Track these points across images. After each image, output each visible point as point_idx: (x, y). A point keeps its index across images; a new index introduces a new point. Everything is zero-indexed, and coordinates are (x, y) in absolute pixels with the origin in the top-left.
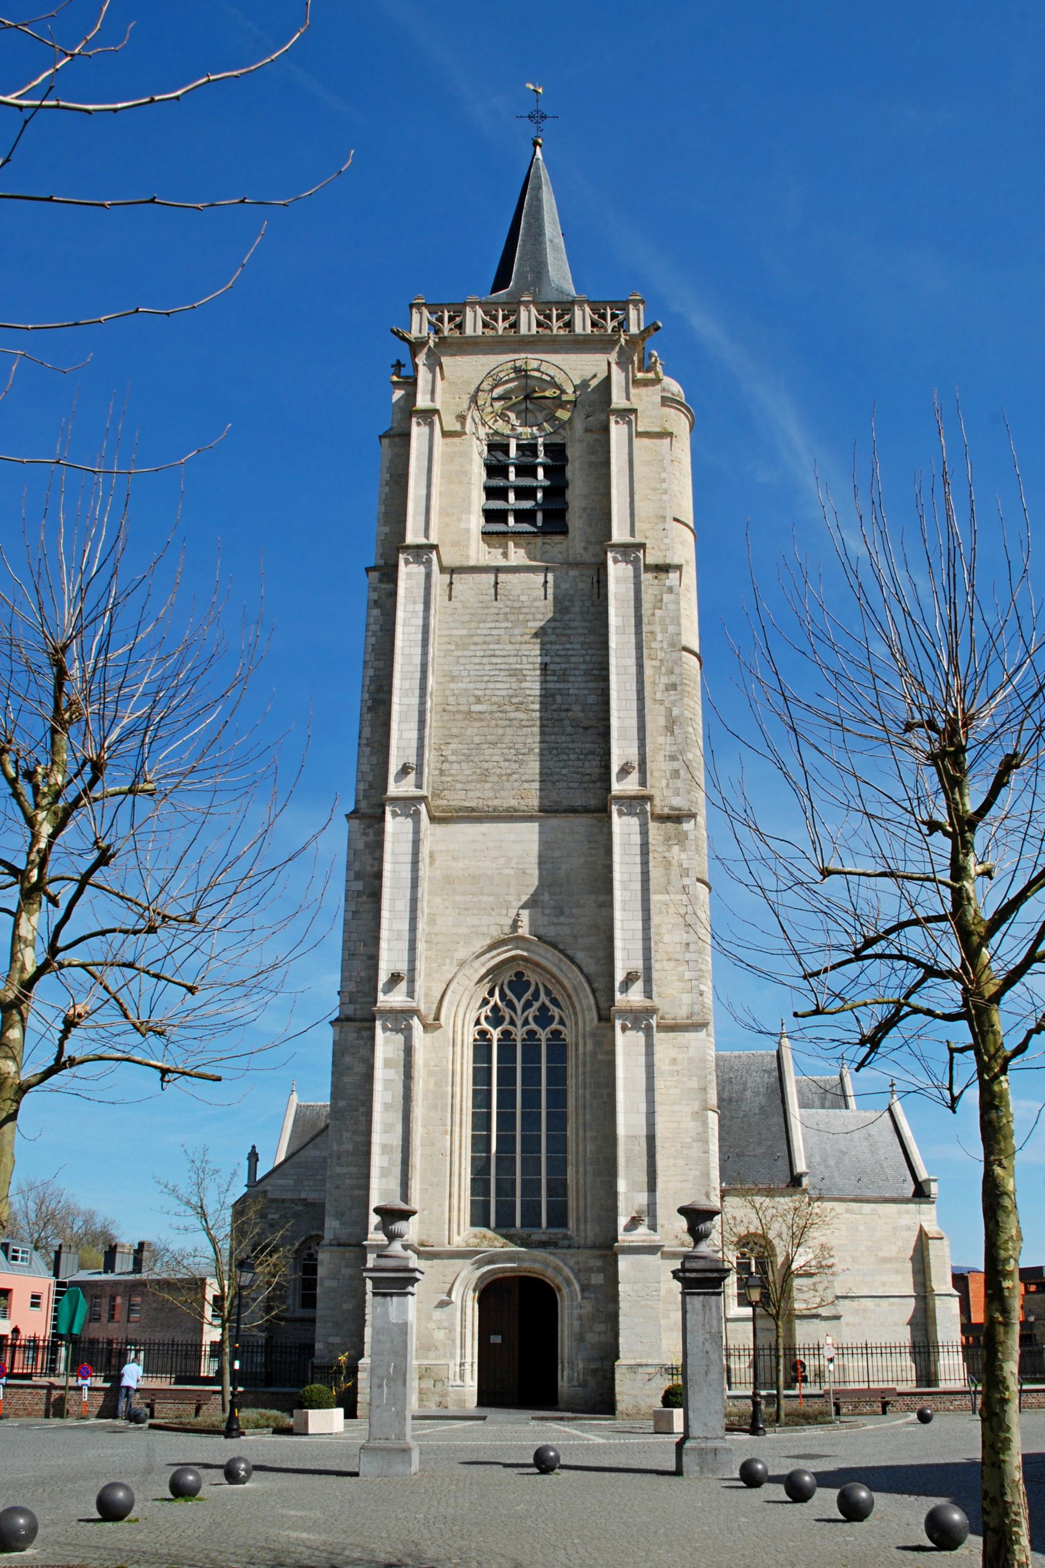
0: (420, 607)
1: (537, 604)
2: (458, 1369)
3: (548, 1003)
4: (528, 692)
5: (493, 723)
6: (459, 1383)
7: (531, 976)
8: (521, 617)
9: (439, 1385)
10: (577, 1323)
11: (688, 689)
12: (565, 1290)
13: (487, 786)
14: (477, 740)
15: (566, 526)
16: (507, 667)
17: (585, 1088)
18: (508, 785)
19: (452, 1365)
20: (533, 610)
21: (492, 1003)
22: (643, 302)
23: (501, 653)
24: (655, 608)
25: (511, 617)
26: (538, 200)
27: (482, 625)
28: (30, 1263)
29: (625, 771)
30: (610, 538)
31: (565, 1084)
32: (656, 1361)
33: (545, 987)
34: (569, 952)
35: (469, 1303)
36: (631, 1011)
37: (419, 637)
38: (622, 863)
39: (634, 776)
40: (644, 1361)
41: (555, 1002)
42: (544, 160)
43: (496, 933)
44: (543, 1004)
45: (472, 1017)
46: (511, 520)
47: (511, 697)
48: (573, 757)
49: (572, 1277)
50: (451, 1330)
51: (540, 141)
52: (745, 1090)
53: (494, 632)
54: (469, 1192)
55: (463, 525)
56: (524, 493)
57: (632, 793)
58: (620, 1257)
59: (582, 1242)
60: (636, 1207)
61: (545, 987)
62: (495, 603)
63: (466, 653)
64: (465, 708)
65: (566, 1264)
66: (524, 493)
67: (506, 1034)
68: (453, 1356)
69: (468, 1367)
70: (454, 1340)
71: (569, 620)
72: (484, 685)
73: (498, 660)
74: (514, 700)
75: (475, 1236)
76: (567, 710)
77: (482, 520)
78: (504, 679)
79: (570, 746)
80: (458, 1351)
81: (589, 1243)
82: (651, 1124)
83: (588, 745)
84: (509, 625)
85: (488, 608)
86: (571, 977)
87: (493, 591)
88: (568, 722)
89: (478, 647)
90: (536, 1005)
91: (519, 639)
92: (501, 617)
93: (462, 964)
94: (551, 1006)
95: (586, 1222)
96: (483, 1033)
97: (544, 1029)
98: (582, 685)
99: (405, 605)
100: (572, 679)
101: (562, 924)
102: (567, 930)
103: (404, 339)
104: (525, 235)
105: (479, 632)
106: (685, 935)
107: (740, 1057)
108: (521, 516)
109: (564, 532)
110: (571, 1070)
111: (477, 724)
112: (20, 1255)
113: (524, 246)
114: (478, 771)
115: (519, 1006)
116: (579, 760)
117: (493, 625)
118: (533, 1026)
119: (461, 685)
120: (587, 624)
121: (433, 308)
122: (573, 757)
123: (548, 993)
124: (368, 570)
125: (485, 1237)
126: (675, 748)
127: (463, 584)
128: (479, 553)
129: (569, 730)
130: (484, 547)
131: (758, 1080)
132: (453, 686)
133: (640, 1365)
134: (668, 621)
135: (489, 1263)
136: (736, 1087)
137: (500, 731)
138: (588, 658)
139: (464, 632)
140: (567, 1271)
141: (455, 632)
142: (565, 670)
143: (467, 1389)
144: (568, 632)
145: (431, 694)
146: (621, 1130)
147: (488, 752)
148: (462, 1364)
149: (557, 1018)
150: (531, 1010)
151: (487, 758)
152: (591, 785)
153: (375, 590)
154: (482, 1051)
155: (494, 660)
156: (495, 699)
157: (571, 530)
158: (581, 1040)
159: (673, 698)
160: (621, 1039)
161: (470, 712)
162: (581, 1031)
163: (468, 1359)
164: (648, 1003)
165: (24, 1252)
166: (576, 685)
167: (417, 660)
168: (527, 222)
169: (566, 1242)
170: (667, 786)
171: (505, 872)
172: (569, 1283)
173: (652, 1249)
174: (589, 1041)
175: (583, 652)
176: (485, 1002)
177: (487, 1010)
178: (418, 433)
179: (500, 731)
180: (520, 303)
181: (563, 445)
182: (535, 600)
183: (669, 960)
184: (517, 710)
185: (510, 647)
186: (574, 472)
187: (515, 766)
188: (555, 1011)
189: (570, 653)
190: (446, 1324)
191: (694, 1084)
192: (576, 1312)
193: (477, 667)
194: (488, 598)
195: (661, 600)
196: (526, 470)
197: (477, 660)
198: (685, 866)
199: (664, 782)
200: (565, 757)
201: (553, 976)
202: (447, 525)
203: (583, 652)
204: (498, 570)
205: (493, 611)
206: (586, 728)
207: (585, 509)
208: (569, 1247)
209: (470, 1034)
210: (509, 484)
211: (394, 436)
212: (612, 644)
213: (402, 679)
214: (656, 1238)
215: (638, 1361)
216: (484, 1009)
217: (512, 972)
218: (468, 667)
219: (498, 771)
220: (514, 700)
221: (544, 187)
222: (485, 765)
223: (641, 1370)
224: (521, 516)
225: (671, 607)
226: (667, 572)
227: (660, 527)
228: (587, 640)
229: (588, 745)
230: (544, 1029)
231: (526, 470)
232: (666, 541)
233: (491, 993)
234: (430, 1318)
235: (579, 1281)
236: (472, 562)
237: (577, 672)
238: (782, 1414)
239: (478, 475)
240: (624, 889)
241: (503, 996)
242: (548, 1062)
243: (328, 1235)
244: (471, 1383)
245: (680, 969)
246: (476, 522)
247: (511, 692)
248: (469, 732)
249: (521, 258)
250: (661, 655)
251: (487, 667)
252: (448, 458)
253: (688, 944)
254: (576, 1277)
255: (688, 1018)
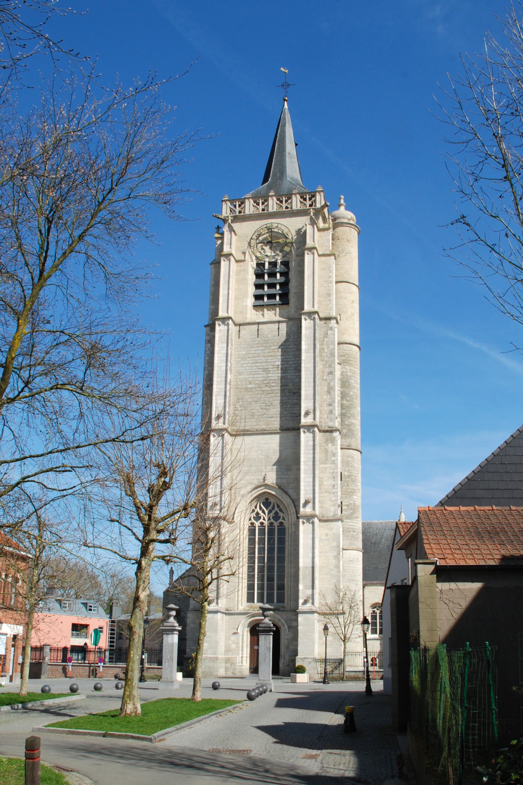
0: (225, 345)
1: (275, 338)
2: (240, 659)
3: (278, 511)
4: (271, 378)
5: (256, 392)
6: (240, 664)
7: (272, 500)
8: (268, 345)
9: (233, 665)
10: (286, 641)
11: (351, 362)
12: (282, 628)
13: (254, 420)
14: (250, 400)
15: (288, 300)
16: (262, 367)
17: (291, 546)
18: (262, 419)
19: (238, 657)
20: (273, 341)
21: (256, 511)
22: (322, 191)
23: (260, 361)
24: (324, 337)
25: (264, 345)
26: (284, 132)
27: (252, 349)
28: (98, 612)
29: (307, 414)
30: (303, 309)
31: (285, 544)
32: (312, 657)
33: (277, 505)
34: (286, 490)
35: (245, 633)
36: (306, 516)
37: (225, 358)
38: (304, 454)
39: (311, 416)
40: (307, 657)
41: (281, 510)
42: (289, 109)
43: (256, 483)
44: (276, 512)
45: (248, 517)
46: (266, 299)
47: (264, 380)
48: (289, 406)
49: (284, 622)
50: (238, 644)
51: (286, 98)
52: (382, 538)
53: (257, 352)
54: (246, 589)
55: (244, 304)
56: (272, 286)
57: (309, 424)
58: (299, 615)
59: (289, 609)
60: (306, 596)
61: (277, 505)
62: (258, 339)
63: (246, 362)
64: (244, 386)
65: (282, 618)
66: (272, 286)
67: (262, 523)
68: (238, 654)
69: (244, 658)
70: (239, 648)
71: (289, 345)
72: (252, 376)
73: (259, 365)
74: (265, 382)
75: (248, 607)
76: (287, 386)
77: (253, 300)
78: (261, 373)
79: (288, 401)
80: (241, 652)
81: (292, 609)
82: (313, 562)
83: (295, 401)
84: (263, 348)
85: (255, 341)
86: (286, 501)
87: (257, 333)
88: (287, 391)
89: (250, 359)
90: (274, 512)
91: (267, 354)
92: (260, 345)
93: (243, 496)
94: (279, 512)
95: (291, 601)
96: (252, 524)
97: (276, 521)
98: (293, 374)
99: (219, 344)
100: (289, 371)
101: (283, 478)
102: (285, 481)
103: (219, 218)
104: (277, 152)
105: (251, 352)
106: (333, 482)
107: (382, 523)
108: (271, 297)
109: (288, 304)
110: (287, 539)
111: (250, 393)
112: (93, 608)
113: (276, 157)
114: (250, 414)
115: (266, 512)
116: (291, 407)
117: (256, 349)
118: (272, 520)
119: (243, 376)
120: (295, 346)
121: (232, 201)
122: (289, 406)
123: (278, 506)
124: (206, 326)
125: (252, 607)
126: (331, 400)
127: (245, 330)
128: (253, 315)
129: (287, 394)
130: (254, 312)
131: (389, 533)
132: (240, 377)
133: (306, 658)
134: (330, 343)
135: (253, 617)
136: (378, 537)
137: (259, 396)
138: (296, 362)
139: (244, 353)
140: (283, 621)
141: (241, 353)
142: (286, 368)
143: (244, 667)
144: (288, 350)
145: (230, 382)
146: (301, 564)
147: (254, 405)
148: (242, 657)
149: (282, 517)
150: (271, 514)
151: (254, 408)
152: (296, 418)
153: (208, 335)
154: (252, 531)
155: (257, 365)
156: (257, 382)
157: (290, 303)
158: (290, 527)
159: (331, 378)
160: (302, 527)
161: (247, 388)
162: (290, 523)
163: (245, 655)
164: (313, 513)
165: (94, 607)
166: (291, 374)
167: (224, 369)
168: (278, 145)
169: (283, 609)
170: (327, 417)
171: (261, 457)
172: (284, 626)
173: (312, 612)
174: (293, 527)
175: (294, 359)
176: (253, 511)
177: (254, 514)
178: (224, 264)
179: (259, 396)
180: (269, 196)
181: (288, 262)
182: (274, 336)
183: (326, 492)
184: (266, 386)
185: (263, 358)
186: (292, 275)
187: (265, 411)
188: (281, 514)
189: (288, 360)
190: (236, 642)
191: (335, 544)
192: (286, 637)
193: (250, 368)
194: (255, 336)
195: (327, 334)
196: (272, 275)
197: (250, 365)
198: (334, 452)
199: (326, 416)
200: (285, 406)
201: (280, 500)
202: (238, 304)
203: (294, 359)
204: (259, 323)
205: (257, 342)
206: (294, 393)
207: (296, 293)
208: (284, 611)
209: (247, 525)
210: (265, 282)
211: (216, 263)
212: (303, 358)
213: (217, 377)
214: (314, 609)
215: (305, 656)
216: (252, 514)
217: (264, 498)
218: (246, 368)
219: (258, 413)
220: (265, 382)
221: (287, 125)
222: (253, 411)
223: (306, 660)
224: (271, 297)
225: (331, 336)
226: (330, 320)
227: (328, 299)
228: (296, 353)
229: (295, 401)
230: (276, 521)
231: (272, 275)
232: (330, 305)
233: (256, 507)
234: (230, 639)
235: (287, 625)
236: (248, 321)
237: (291, 368)
238: (345, 677)
239: (252, 278)
240: (305, 465)
241: (260, 508)
242: (278, 535)
243: (191, 607)
244: (245, 664)
245: (331, 496)
246: (250, 301)
247: (264, 379)
248: (247, 397)
249: (275, 165)
250: (326, 359)
251: (254, 368)
252: (238, 273)
253: (334, 486)
254: (286, 623)
255: (333, 517)
